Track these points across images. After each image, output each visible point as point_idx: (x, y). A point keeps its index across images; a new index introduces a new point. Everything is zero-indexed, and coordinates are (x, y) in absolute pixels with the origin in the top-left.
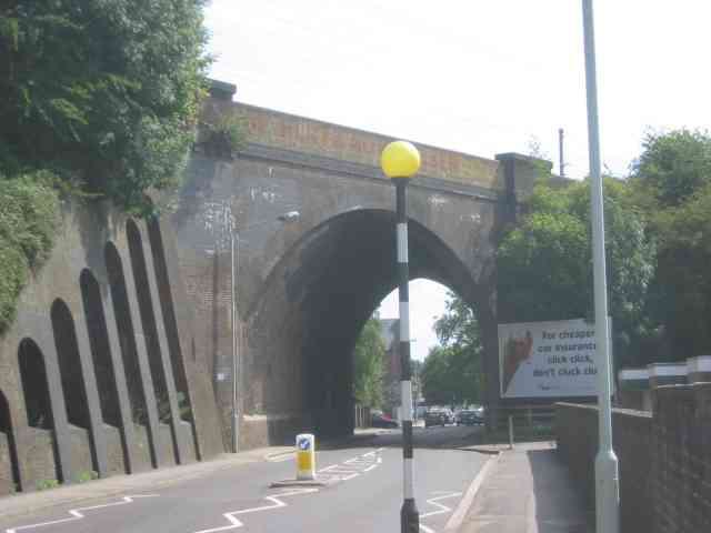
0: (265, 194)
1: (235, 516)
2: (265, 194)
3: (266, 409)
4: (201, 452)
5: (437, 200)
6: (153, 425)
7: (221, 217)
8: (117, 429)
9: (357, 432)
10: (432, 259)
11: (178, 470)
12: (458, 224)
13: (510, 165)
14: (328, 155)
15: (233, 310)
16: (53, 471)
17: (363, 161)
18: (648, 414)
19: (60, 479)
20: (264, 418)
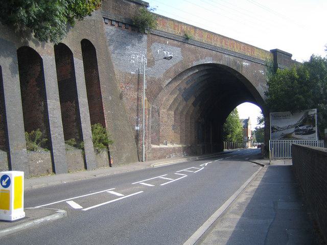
0: (165, 52)
1: (74, 200)
2: (165, 52)
3: (181, 143)
4: (112, 163)
5: (245, 64)
6: (87, 152)
7: (140, 58)
8: (6, 153)
9: (225, 150)
10: (253, 97)
11: (86, 172)
12: (260, 80)
13: (275, 52)
14: (196, 39)
15: (144, 98)
16: (83, 166)
17: (213, 44)
18: (17, 212)
19: (86, 168)
20: (180, 146)
